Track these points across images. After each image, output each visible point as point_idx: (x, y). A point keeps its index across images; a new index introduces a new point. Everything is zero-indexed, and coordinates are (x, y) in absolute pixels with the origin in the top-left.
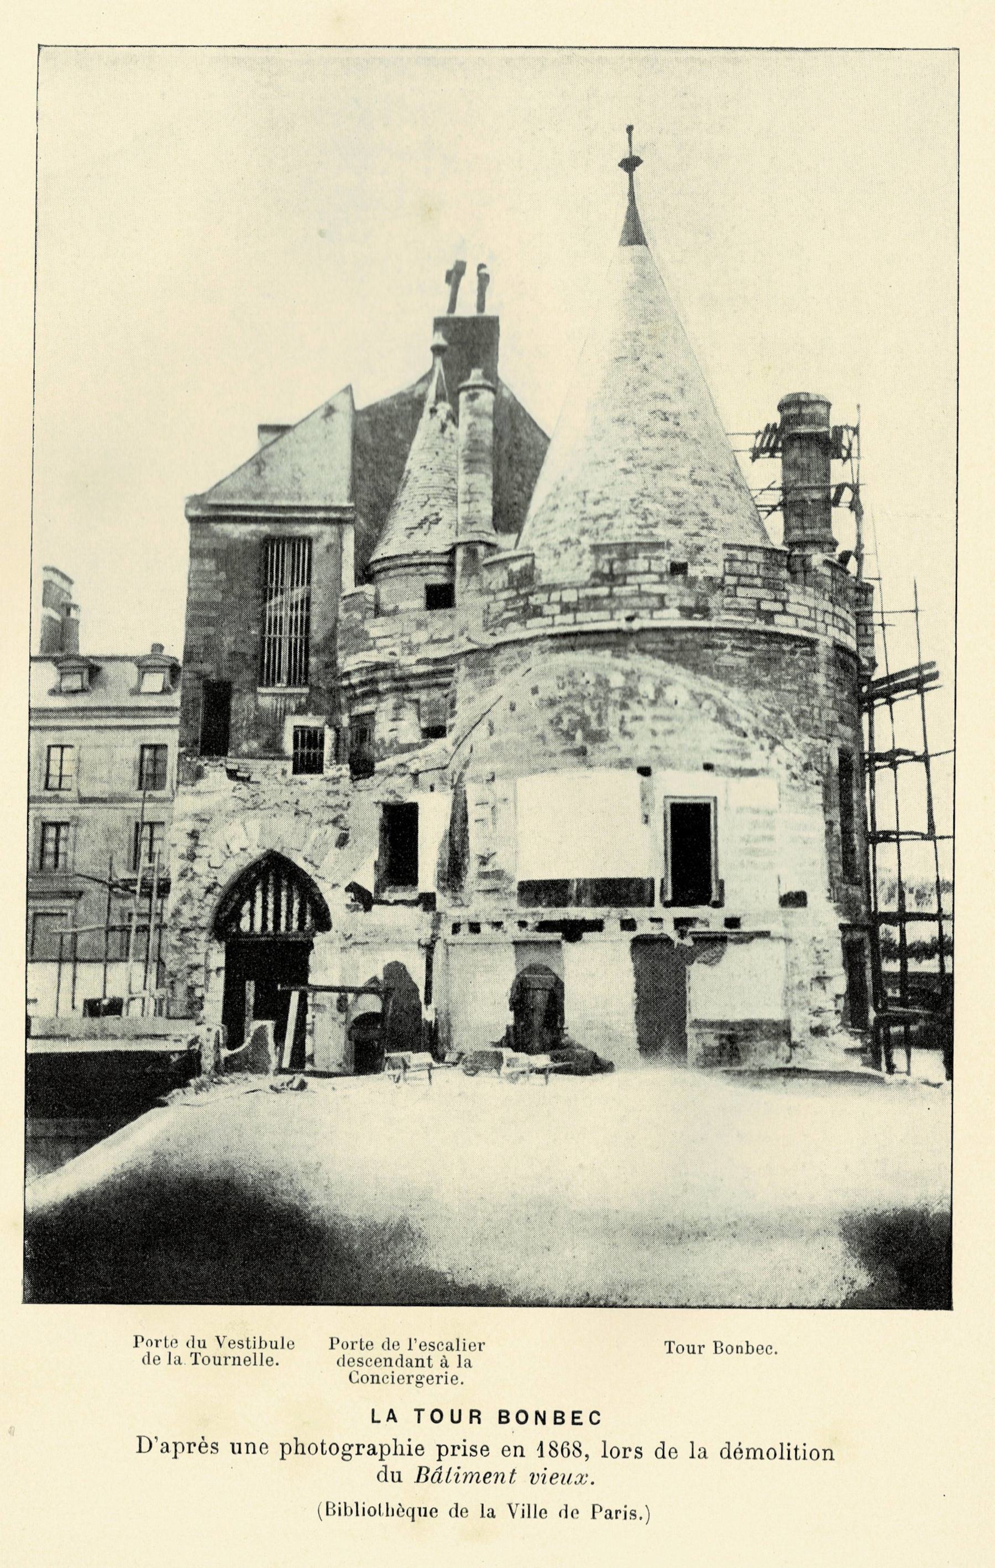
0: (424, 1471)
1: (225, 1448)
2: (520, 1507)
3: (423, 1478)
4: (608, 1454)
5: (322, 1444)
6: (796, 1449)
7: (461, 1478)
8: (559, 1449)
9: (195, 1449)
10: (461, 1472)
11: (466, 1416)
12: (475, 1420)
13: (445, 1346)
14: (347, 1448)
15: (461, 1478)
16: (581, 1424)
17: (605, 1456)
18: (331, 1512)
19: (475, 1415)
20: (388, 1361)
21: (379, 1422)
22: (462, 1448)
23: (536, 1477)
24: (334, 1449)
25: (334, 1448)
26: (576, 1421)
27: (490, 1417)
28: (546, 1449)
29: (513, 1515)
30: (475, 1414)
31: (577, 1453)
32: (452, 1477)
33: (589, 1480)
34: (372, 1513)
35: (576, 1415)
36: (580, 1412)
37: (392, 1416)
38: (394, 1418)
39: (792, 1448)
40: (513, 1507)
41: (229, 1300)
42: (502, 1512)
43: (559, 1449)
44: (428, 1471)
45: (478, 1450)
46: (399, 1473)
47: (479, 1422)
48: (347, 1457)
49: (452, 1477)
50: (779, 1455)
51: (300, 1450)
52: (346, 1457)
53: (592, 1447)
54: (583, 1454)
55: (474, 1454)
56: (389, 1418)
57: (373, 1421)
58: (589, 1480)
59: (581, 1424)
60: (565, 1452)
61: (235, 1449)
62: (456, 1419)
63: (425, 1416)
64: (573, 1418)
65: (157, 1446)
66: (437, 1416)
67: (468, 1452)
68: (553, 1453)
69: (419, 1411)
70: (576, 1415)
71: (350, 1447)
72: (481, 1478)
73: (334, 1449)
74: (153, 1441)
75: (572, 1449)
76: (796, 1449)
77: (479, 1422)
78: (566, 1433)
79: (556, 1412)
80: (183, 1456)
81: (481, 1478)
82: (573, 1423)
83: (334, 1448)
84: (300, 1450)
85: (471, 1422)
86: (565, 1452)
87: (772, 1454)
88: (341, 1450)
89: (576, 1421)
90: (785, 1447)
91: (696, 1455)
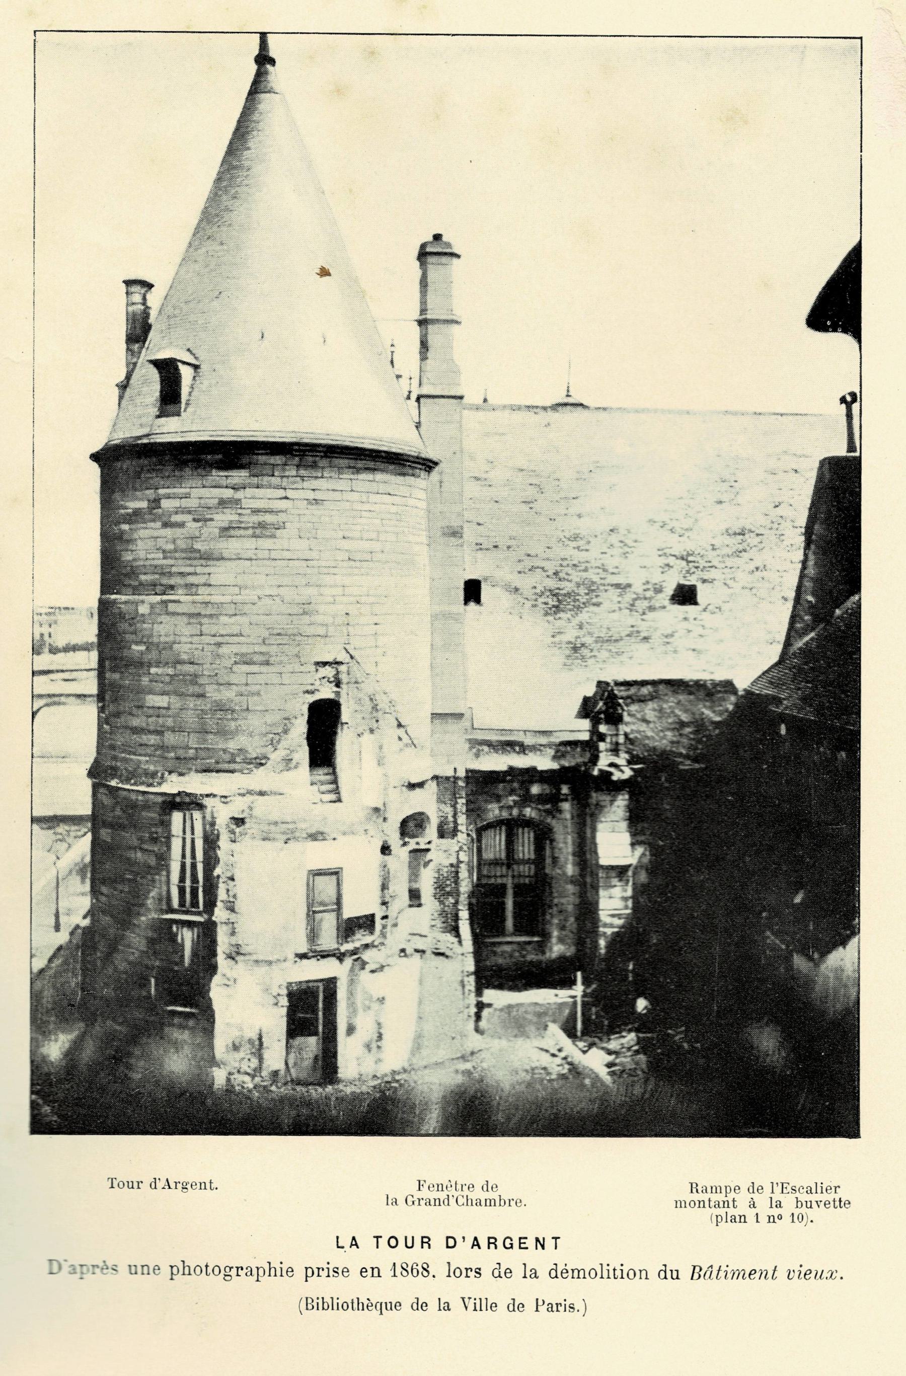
0: (697, 1269)
1: (123, 1269)
2: (472, 1301)
3: (696, 1276)
4: (452, 1274)
5: (207, 1266)
6: (614, 1270)
7: (730, 1275)
8: (409, 1269)
9: (97, 1271)
10: (729, 1270)
11: (418, 1242)
12: (426, 1245)
13: (805, 1190)
14: (227, 1269)
15: (730, 1275)
16: (527, 1248)
17: (449, 1276)
18: (310, 1307)
19: (426, 1241)
20: (203, 1185)
21: (343, 1247)
22: (326, 1270)
23: (792, 1273)
24: (217, 1270)
25: (217, 1269)
26: (522, 1246)
27: (438, 1242)
28: (399, 1270)
29: (466, 1308)
30: (492, 1241)
31: (425, 1273)
32: (722, 1274)
33: (838, 1275)
34: (345, 1307)
35: (522, 1241)
36: (526, 1238)
37: (354, 1243)
38: (356, 1245)
39: (611, 1268)
40: (466, 1300)
41: (725, 1132)
42: (457, 1305)
43: (409, 1269)
44: (701, 1270)
45: (340, 1271)
46: (677, 1271)
47: (496, 1248)
48: (228, 1278)
49: (722, 1274)
50: (599, 1275)
51: (187, 1272)
52: (227, 1278)
53: (438, 1268)
54: (431, 1275)
55: (336, 1275)
56: (352, 1245)
57: (338, 1247)
58: (838, 1275)
59: (527, 1248)
60: (415, 1272)
61: (133, 1270)
62: (409, 1244)
63: (383, 1242)
64: (520, 1243)
65: (66, 1268)
66: (393, 1242)
67: (331, 1273)
68: (405, 1273)
69: (377, 1237)
70: (522, 1241)
71: (231, 1268)
72: (747, 1275)
73: (217, 1270)
74: (63, 1263)
75: (421, 1270)
76: (614, 1270)
77: (496, 1248)
78: (417, 1255)
79: (423, 1238)
80: (88, 1276)
81: (747, 1275)
82: (520, 1248)
83: (217, 1269)
84: (187, 1272)
85: (489, 1248)
86: (415, 1272)
87: (593, 1274)
88: (223, 1272)
89: (522, 1246)
90: (605, 1267)
91: (528, 1275)
